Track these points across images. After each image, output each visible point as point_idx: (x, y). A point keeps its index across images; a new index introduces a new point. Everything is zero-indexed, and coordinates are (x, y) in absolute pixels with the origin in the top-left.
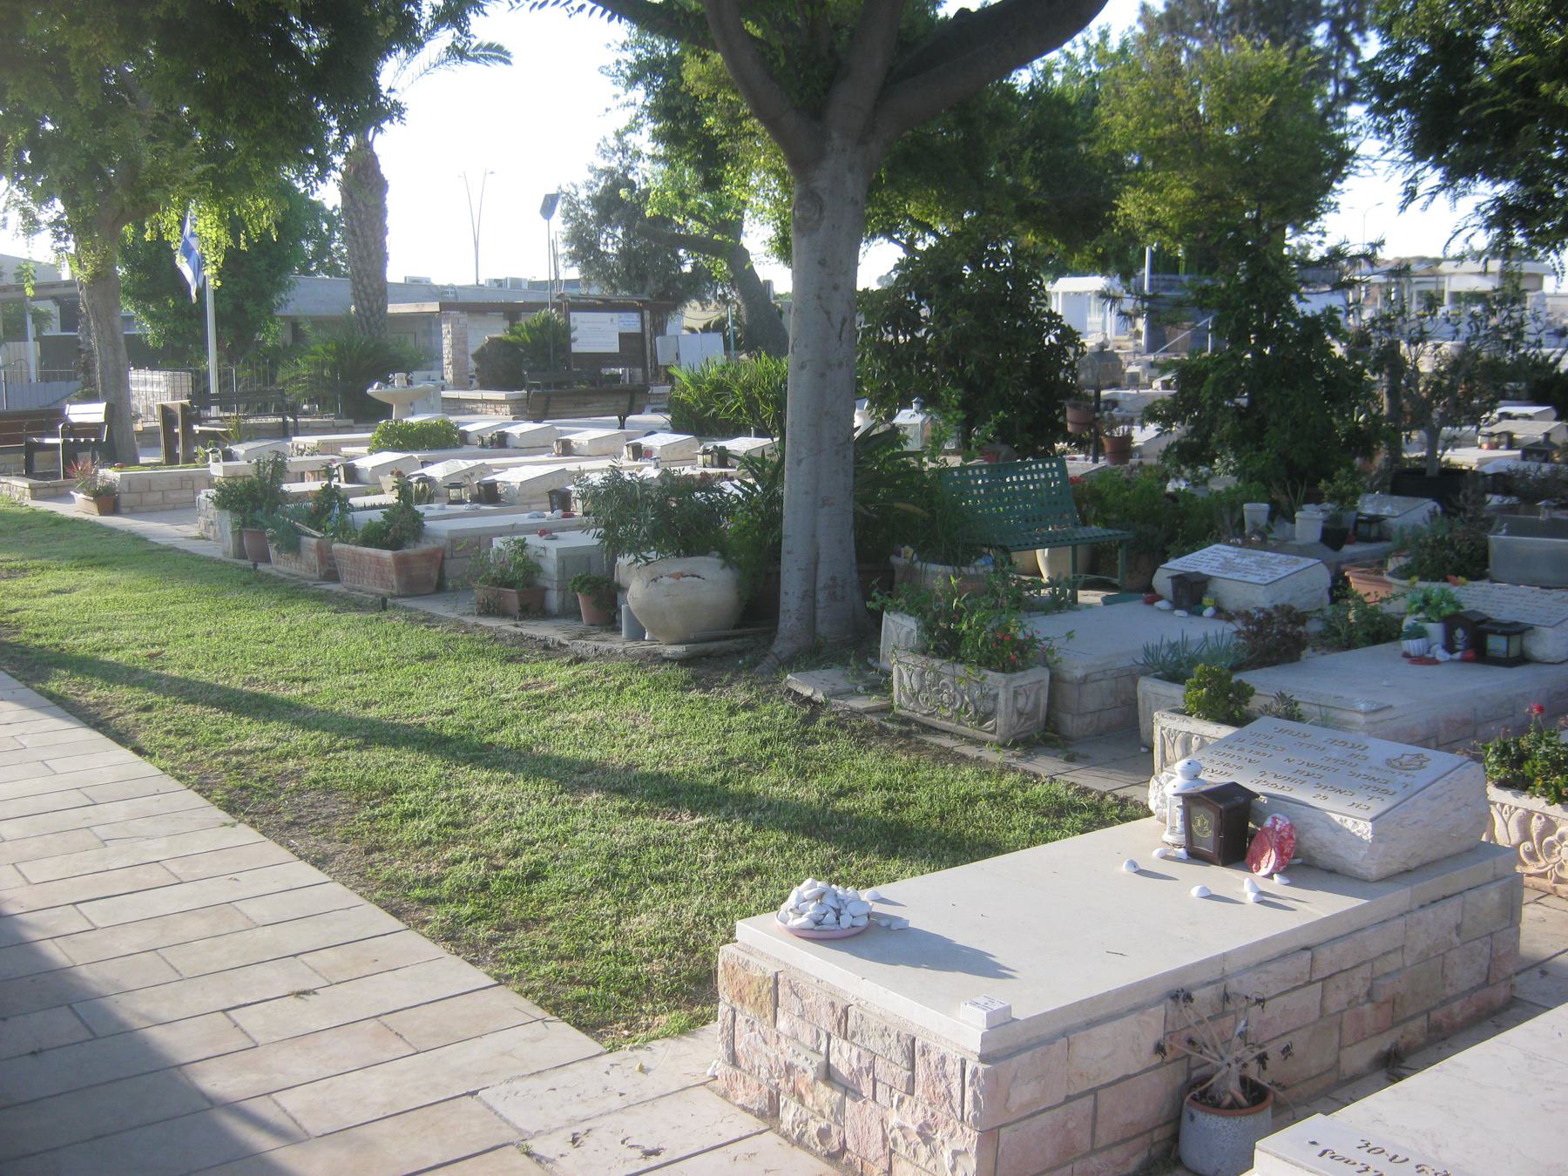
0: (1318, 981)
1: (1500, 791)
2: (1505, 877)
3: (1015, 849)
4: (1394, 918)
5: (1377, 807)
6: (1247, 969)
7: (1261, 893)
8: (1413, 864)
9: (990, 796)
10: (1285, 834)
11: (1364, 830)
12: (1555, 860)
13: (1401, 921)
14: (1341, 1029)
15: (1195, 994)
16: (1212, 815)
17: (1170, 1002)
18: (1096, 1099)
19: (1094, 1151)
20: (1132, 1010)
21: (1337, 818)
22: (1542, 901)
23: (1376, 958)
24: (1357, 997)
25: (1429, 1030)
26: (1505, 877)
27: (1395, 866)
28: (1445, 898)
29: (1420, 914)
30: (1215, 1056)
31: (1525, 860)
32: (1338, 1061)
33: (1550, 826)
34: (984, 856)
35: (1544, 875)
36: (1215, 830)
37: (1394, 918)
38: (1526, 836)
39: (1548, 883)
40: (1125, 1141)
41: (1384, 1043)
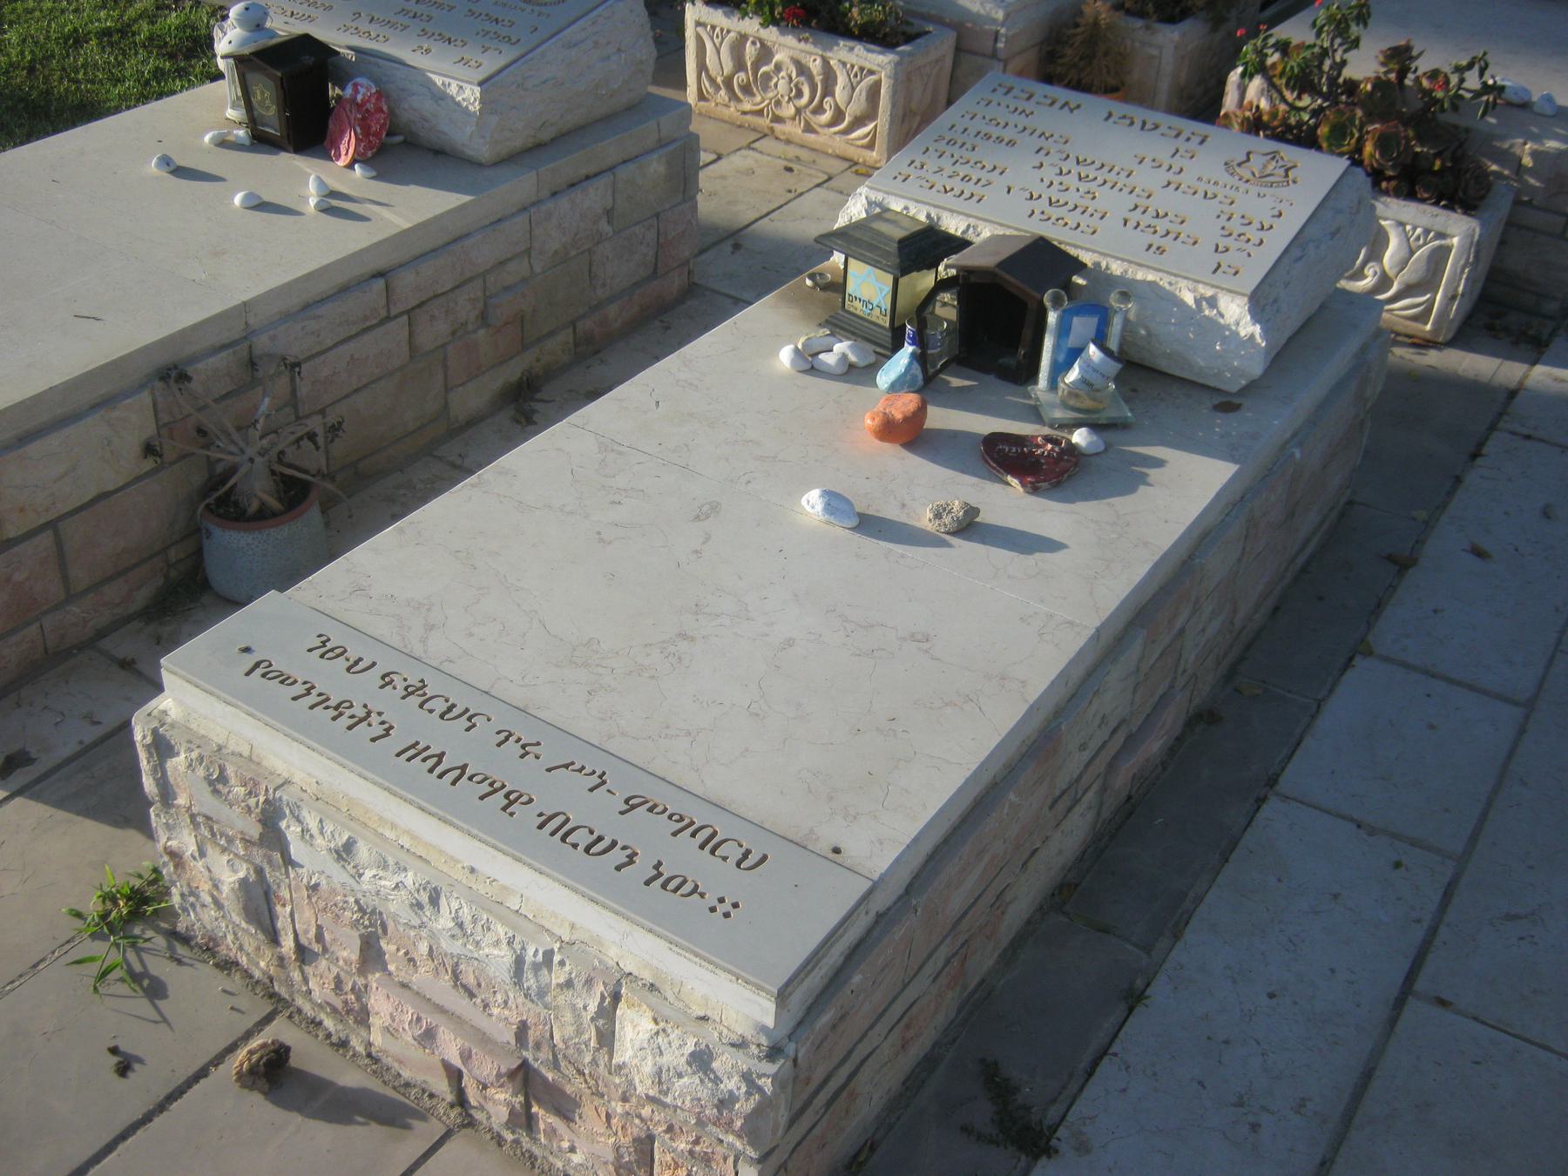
0: (401, 314)
1: (711, 10)
2: (675, 140)
3: (117, 110)
4: (513, 215)
5: (491, 63)
6: (287, 316)
7: (334, 194)
8: (545, 136)
9: (107, 33)
10: (370, 106)
11: (469, 95)
12: (771, 95)
13: (522, 220)
14: (445, 367)
15: (190, 371)
16: (270, 83)
17: (159, 385)
18: (484, 282)
19: (71, 597)
20: (95, 407)
21: (438, 80)
22: (756, 145)
23: (488, 271)
24: (464, 324)
25: (576, 345)
26: (675, 140)
27: (518, 143)
28: (588, 178)
29: (550, 205)
30: (232, 448)
31: (740, 94)
32: (446, 406)
33: (765, 53)
34: (73, 124)
35: (760, 113)
36: (278, 106)
37: (513, 215)
38: (739, 65)
39: (764, 122)
40: (120, 574)
41: (513, 372)
